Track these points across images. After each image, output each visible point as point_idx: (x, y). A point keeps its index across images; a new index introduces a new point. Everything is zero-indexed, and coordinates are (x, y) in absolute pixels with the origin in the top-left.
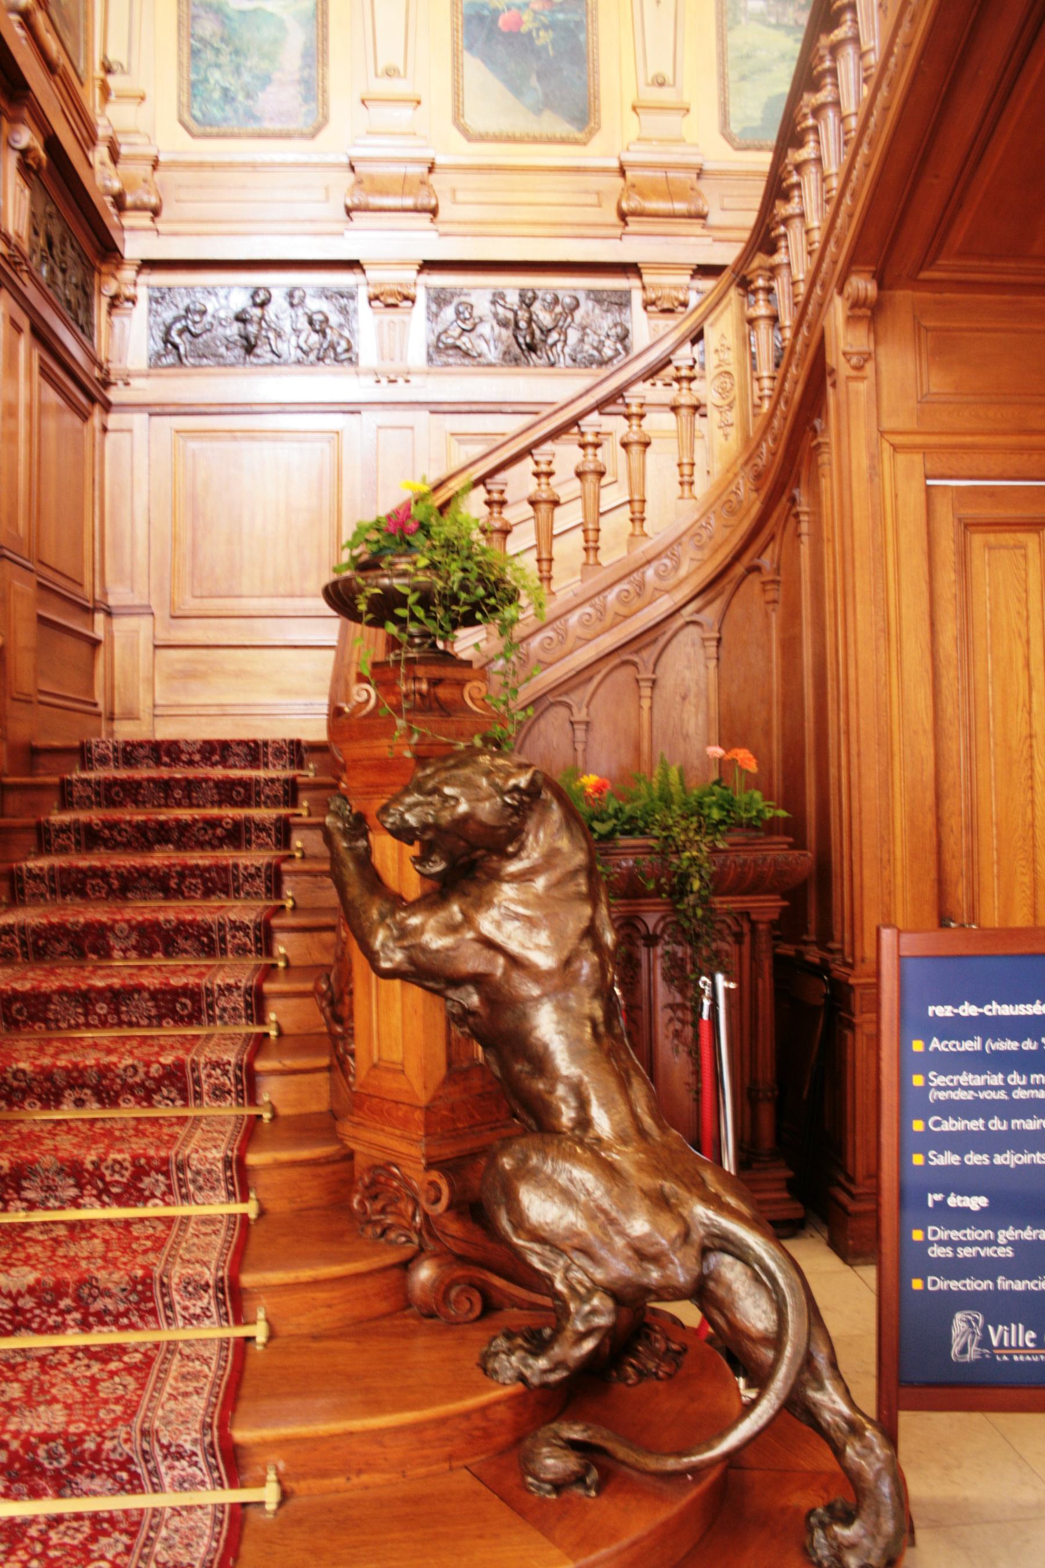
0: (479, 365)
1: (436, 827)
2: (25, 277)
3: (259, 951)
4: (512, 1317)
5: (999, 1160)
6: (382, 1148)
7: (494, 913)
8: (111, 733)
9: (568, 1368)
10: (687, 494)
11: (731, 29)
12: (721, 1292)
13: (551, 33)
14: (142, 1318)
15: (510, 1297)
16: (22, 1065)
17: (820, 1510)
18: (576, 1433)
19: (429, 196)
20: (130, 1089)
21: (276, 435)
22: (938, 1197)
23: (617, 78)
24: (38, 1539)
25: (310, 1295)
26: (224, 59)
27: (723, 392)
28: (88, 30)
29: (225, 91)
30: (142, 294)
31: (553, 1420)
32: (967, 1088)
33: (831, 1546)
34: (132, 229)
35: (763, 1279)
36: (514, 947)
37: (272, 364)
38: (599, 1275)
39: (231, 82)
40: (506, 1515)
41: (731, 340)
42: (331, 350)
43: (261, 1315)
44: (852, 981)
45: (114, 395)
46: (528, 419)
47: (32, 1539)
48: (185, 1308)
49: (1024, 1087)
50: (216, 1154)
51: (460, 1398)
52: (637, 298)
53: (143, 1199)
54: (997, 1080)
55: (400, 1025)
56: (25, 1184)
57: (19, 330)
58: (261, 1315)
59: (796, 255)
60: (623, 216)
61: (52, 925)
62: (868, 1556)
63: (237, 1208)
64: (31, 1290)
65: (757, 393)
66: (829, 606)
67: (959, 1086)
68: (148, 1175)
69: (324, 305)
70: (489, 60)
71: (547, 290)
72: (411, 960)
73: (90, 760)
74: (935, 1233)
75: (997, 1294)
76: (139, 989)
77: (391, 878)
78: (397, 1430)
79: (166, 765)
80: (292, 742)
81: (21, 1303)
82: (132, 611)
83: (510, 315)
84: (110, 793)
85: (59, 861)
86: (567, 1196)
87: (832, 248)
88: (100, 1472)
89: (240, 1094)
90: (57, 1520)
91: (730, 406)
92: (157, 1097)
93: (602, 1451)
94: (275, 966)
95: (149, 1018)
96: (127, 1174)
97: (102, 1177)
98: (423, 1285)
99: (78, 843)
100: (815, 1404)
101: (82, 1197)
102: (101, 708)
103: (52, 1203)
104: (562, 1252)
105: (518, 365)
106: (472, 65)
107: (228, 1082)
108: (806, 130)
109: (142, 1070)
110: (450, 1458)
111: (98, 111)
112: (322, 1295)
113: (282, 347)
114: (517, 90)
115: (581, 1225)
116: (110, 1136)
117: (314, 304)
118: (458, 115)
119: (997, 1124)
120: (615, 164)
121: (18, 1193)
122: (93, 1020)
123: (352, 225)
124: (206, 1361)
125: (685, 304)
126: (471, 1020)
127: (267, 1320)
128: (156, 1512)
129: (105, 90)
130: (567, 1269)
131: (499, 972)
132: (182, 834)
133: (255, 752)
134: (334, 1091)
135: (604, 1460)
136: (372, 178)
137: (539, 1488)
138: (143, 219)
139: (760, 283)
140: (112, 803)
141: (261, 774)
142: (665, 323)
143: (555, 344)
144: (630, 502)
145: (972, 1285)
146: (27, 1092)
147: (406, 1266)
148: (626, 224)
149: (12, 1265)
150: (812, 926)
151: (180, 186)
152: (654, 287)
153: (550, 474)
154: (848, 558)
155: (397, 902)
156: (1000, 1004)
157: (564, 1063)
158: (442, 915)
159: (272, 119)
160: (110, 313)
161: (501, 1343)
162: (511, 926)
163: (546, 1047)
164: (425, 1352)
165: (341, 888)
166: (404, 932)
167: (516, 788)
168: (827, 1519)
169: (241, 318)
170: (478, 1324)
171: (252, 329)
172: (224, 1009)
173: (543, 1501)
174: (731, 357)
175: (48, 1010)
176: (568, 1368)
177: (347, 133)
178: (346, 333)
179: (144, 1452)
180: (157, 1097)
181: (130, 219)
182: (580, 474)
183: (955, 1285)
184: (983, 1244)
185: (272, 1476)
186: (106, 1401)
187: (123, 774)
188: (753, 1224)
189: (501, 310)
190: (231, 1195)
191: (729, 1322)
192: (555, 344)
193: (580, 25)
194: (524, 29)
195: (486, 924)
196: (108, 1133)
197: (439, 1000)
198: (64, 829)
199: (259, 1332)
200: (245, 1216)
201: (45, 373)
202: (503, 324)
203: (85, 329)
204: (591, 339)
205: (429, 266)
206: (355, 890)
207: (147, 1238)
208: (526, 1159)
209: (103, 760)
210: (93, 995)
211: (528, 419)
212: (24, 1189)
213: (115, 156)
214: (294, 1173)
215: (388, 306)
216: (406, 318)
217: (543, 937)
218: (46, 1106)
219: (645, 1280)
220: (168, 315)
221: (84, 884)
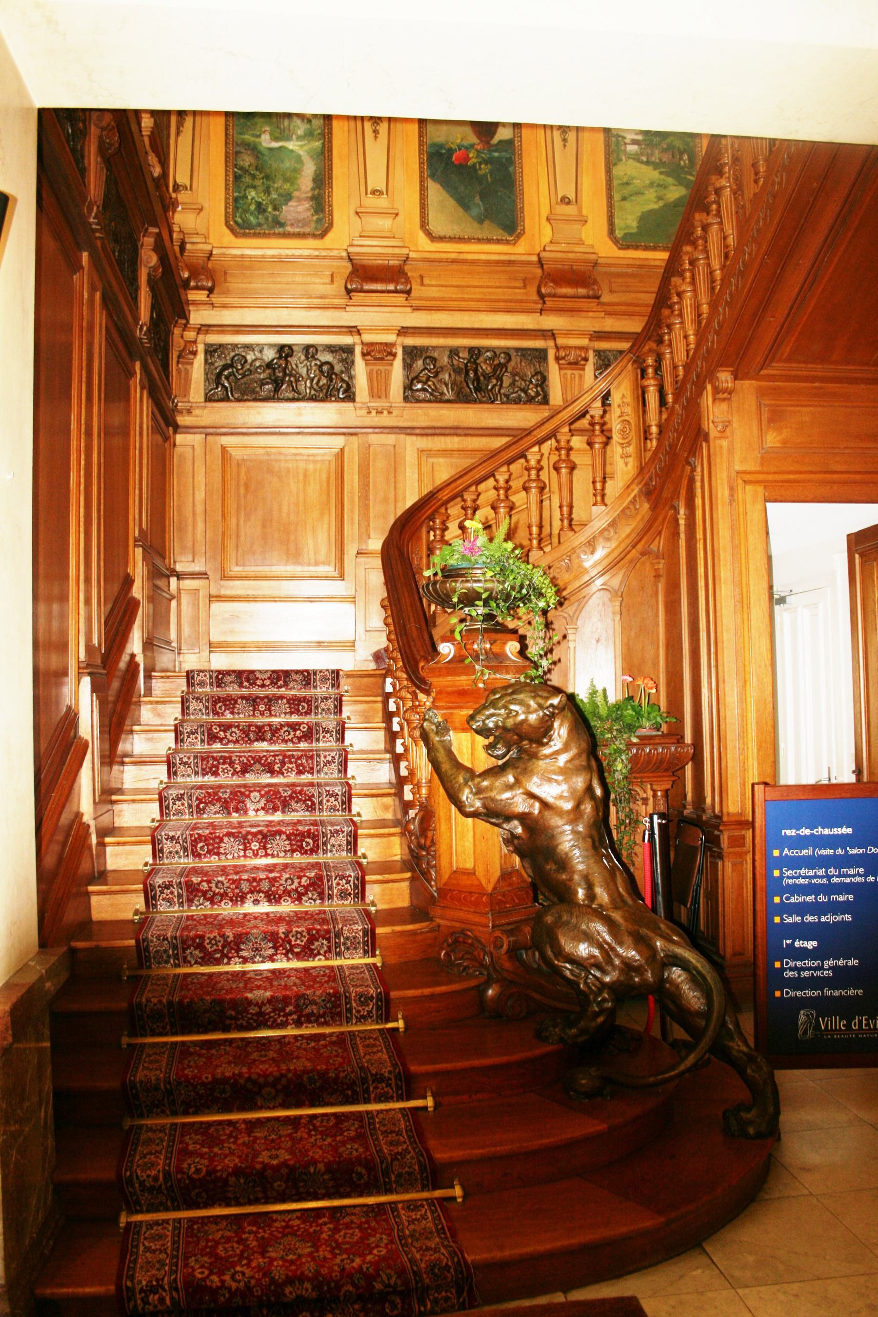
1: (505, 729)
3: (344, 810)
5: (823, 919)
6: (462, 921)
7: (535, 779)
11: (615, 164)
13: (489, 166)
14: (332, 1018)
20: (287, 893)
22: (789, 942)
26: (258, 182)
29: (259, 205)
30: (201, 348)
32: (805, 877)
34: (194, 303)
39: (262, 198)
43: (400, 1016)
45: (181, 420)
48: (358, 1012)
49: (837, 876)
54: (821, 872)
55: (472, 846)
58: (400, 1016)
63: (370, 960)
64: (270, 1001)
67: (800, 876)
70: (447, 185)
72: (484, 806)
74: (787, 963)
75: (823, 998)
77: (465, 759)
80: (333, 672)
86: (588, 937)
89: (356, 896)
92: (304, 898)
95: (285, 851)
96: (305, 940)
97: (290, 942)
101: (276, 954)
103: (258, 958)
106: (434, 189)
109: (296, 881)
114: (464, 203)
115: (596, 952)
118: (424, 224)
119: (822, 898)
121: (237, 952)
122: (249, 853)
123: (351, 302)
126: (516, 841)
130: (587, 978)
131: (536, 812)
145: (809, 993)
146: (223, 896)
148: (544, 303)
152: (565, 348)
156: (823, 828)
159: (292, 225)
167: (552, 705)
172: (333, 846)
174: (628, 410)
177: (347, 234)
179: (362, 1079)
180: (304, 898)
183: (799, 993)
184: (816, 969)
190: (366, 952)
193: (510, 161)
195: (535, 785)
205: (403, 331)
208: (560, 917)
212: (241, 950)
215: (376, 359)
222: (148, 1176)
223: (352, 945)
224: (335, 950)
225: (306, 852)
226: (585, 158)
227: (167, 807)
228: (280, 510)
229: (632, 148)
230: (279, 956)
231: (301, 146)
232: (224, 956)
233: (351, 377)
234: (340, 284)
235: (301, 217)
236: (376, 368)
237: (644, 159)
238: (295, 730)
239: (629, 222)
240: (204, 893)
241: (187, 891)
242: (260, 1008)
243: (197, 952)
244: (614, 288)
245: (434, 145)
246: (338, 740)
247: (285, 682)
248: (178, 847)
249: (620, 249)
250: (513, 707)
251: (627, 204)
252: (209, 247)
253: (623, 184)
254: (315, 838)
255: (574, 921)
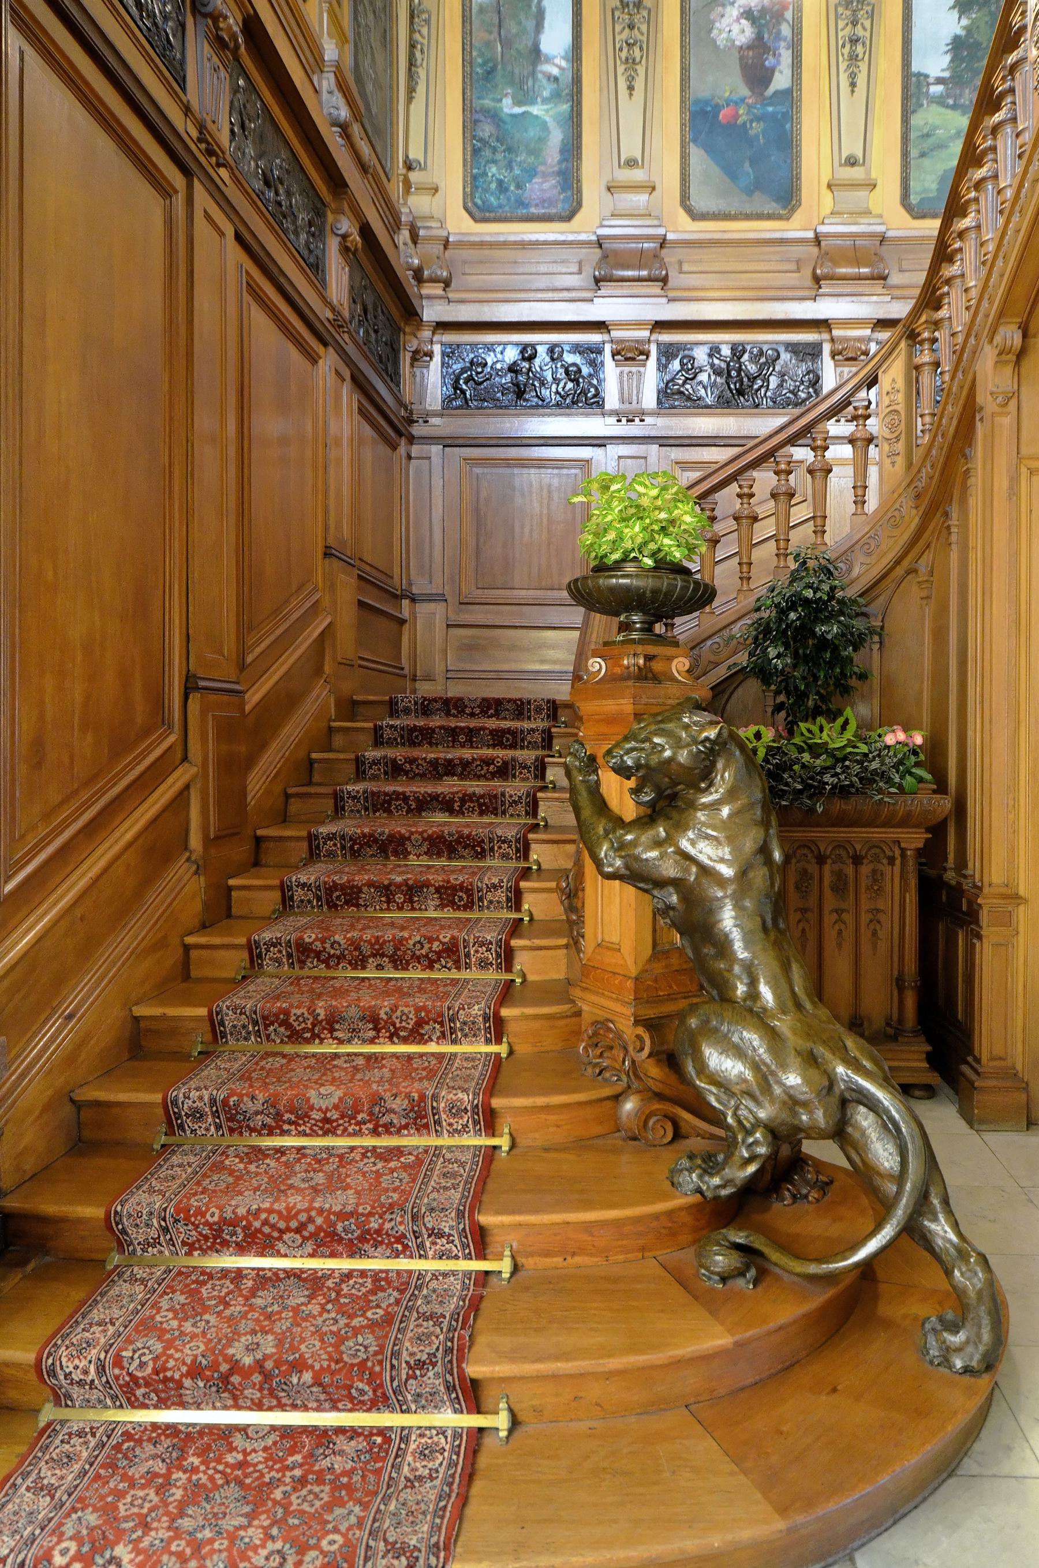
0: (699, 407)
2: (346, 336)
4: (694, 1143)
7: (691, 834)
8: (414, 691)
9: (735, 1186)
10: (859, 511)
11: (914, 112)
12: (857, 1135)
15: (694, 1128)
16: (337, 938)
17: (933, 1319)
18: (740, 1238)
19: (661, 268)
21: (542, 463)
23: (816, 162)
24: (333, 1289)
25: (543, 1116)
26: (499, 156)
27: (892, 427)
28: (394, 135)
29: (500, 182)
30: (437, 349)
31: (724, 1227)
33: (941, 1349)
34: (429, 297)
35: (890, 1128)
36: (704, 859)
37: (537, 406)
38: (762, 1114)
39: (504, 175)
40: (683, 1296)
41: (900, 384)
42: (584, 396)
43: (506, 1130)
44: (979, 901)
45: (417, 430)
46: (737, 450)
47: (329, 1289)
50: (476, 1010)
51: (653, 1203)
52: (827, 348)
53: (422, 1040)
56: (337, 1026)
57: (343, 380)
59: (955, 310)
60: (817, 280)
61: (364, 835)
62: (971, 1359)
63: (493, 1048)
65: (920, 427)
66: (971, 602)
68: (427, 1023)
69: (576, 359)
70: (709, 149)
71: (754, 343)
72: (627, 867)
73: (397, 711)
76: (427, 884)
77: (614, 803)
78: (603, 1224)
79: (454, 716)
80: (549, 701)
81: (329, 1115)
82: (430, 598)
83: (723, 365)
84: (413, 737)
85: (372, 786)
86: (739, 1052)
87: (985, 304)
88: (382, 1243)
90: (349, 1275)
91: (898, 439)
92: (437, 966)
93: (759, 1254)
94: (530, 868)
96: (412, 1023)
98: (629, 1114)
99: (386, 773)
100: (930, 1231)
102: (406, 671)
104: (733, 1094)
105: (729, 407)
106: (696, 154)
107: (491, 957)
108: (968, 201)
110: (643, 1249)
111: (401, 201)
112: (553, 1118)
113: (545, 393)
114: (732, 173)
115: (749, 1075)
116: (399, 991)
117: (570, 358)
120: (810, 235)
123: (599, 293)
124: (462, 1165)
125: (866, 353)
126: (671, 913)
127: (511, 1134)
128: (421, 1275)
129: (407, 184)
130: (737, 1108)
132: (464, 769)
133: (521, 708)
134: (570, 965)
135: (760, 1261)
136: (615, 252)
137: (709, 1279)
138: (437, 290)
139: (926, 335)
140: (413, 744)
141: (526, 725)
142: (847, 370)
143: (759, 389)
144: (813, 517)
146: (340, 958)
147: (617, 1098)
149: (323, 1085)
150: (951, 857)
151: (465, 262)
153: (752, 495)
154: (988, 562)
155: (619, 822)
157: (740, 950)
158: (651, 833)
159: (537, 205)
160: (412, 365)
161: (685, 1163)
162: (702, 845)
163: (727, 935)
164: (629, 1164)
165: (577, 811)
166: (622, 846)
167: (707, 739)
168: (939, 1327)
169: (513, 369)
170: (670, 1147)
171: (522, 378)
172: (491, 902)
173: (713, 1289)
175: (359, 898)
176: (735, 1186)
178: (595, 382)
179: (414, 1232)
180: (437, 966)
181: (427, 290)
182: (774, 496)
185: (507, 1253)
186: (387, 1190)
187: (420, 723)
188: (885, 1082)
189: (716, 361)
191: (863, 1160)
192: (759, 389)
194: (740, 121)
196: (399, 990)
197: (648, 897)
198: (375, 762)
199: (503, 1142)
200: (498, 1055)
201: (362, 412)
202: (718, 372)
203: (393, 377)
204: (790, 384)
205: (659, 326)
206: (587, 812)
207: (424, 1069)
208: (707, 1022)
209: (407, 711)
210: (393, 888)
211: (737, 450)
213: (415, 238)
214: (536, 1025)
215: (627, 359)
216: (642, 369)
217: (726, 852)
218: (355, 968)
219: (796, 1122)
220: (457, 367)
221: (390, 804)
222: (76, 1367)
223: (471, 1032)
224: (449, 1035)
225: (458, 908)
226: (878, 105)
227: (318, 847)
228: (522, 527)
229: (936, 89)
230: (382, 1040)
231: (547, 111)
232: (315, 1036)
233: (599, 381)
234: (589, 272)
235: (547, 195)
236: (627, 369)
237: (951, 102)
238: (488, 764)
239: (927, 184)
240: (318, 954)
241: (298, 951)
242: (325, 1113)
243: (282, 1029)
244: (905, 265)
245: (697, 101)
246: (536, 777)
247: (496, 710)
248: (310, 896)
249: (914, 218)
250: (657, 740)
251: (926, 162)
252: (445, 234)
253: (923, 136)
254: (469, 892)
255: (724, 1028)
